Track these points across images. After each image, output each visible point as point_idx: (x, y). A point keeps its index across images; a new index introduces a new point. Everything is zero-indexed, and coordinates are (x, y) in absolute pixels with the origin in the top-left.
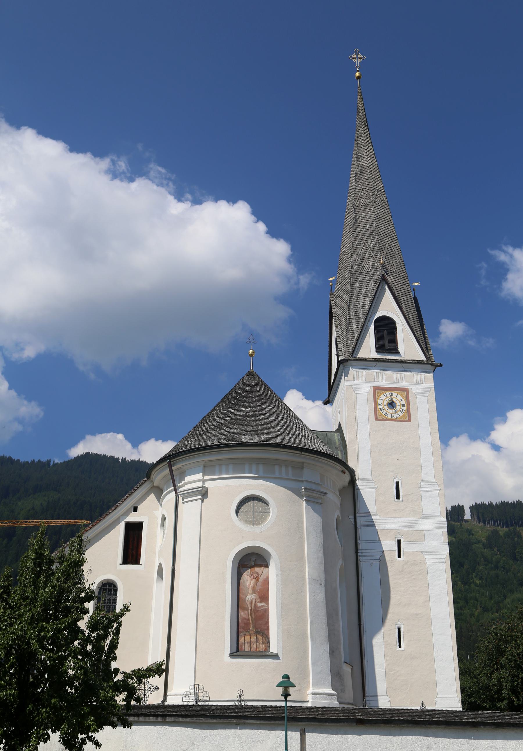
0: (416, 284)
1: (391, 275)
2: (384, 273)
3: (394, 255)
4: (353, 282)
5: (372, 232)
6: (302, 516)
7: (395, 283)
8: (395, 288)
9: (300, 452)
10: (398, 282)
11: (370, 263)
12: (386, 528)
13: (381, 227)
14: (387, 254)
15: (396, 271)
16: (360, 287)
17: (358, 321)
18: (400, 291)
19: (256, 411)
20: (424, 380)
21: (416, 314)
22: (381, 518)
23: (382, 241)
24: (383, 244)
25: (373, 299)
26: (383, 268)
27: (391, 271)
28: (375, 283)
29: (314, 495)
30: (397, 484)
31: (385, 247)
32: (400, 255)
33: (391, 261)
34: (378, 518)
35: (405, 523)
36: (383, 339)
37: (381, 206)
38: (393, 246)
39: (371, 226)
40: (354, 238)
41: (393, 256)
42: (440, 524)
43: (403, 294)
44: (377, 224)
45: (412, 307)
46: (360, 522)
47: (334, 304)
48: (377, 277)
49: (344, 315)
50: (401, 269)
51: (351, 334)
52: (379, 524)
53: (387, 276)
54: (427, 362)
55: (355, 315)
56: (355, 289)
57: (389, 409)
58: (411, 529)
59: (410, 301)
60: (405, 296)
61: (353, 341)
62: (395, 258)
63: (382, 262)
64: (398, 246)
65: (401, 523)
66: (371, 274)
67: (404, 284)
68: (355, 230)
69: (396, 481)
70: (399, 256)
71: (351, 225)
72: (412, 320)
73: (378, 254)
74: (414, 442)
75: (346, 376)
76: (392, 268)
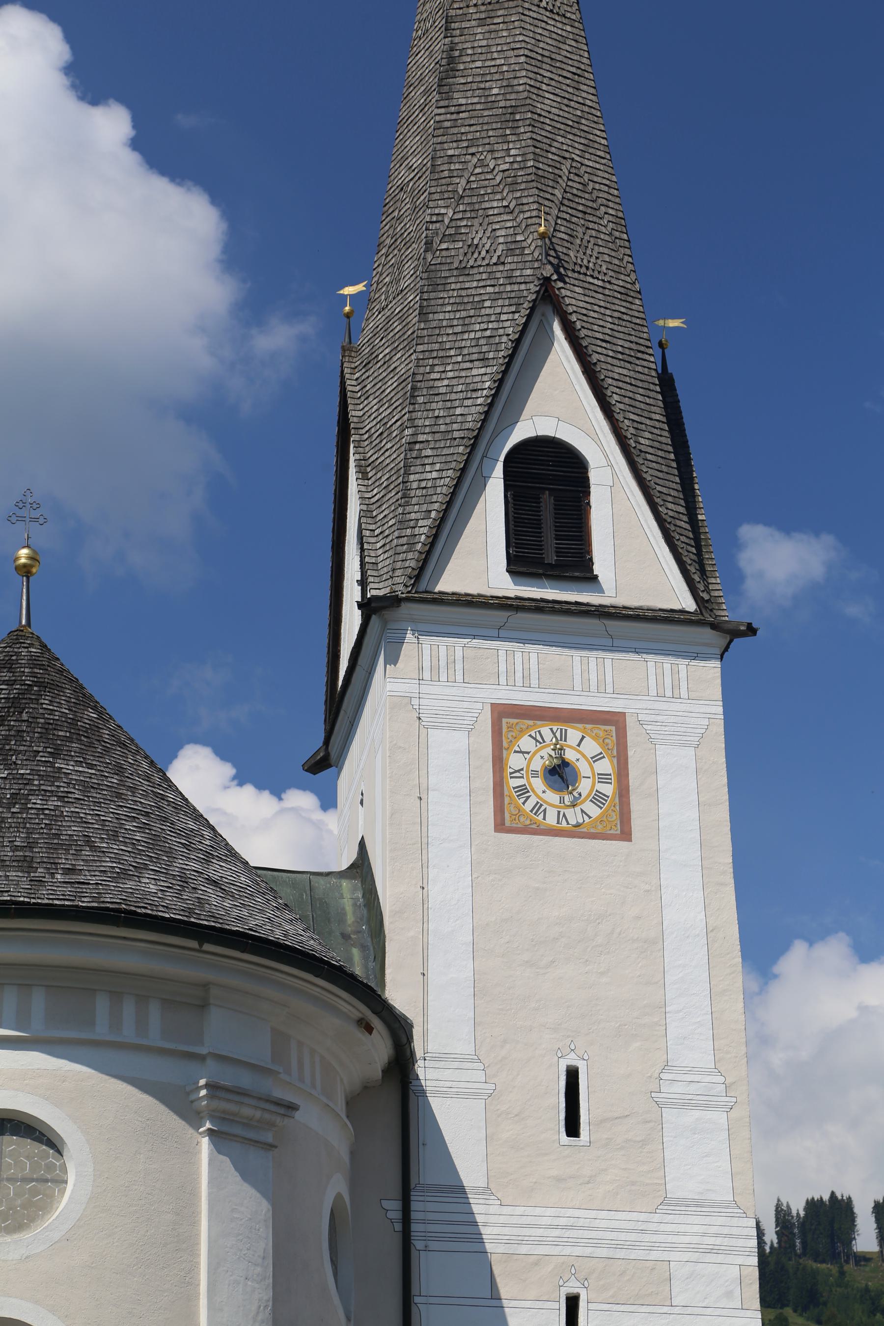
0: (673, 323)
1: (576, 283)
2: (548, 271)
3: (590, 204)
4: (432, 302)
5: (510, 110)
6: (194, 1194)
7: (592, 314)
8: (590, 333)
9: (194, 944)
10: (602, 310)
11: (498, 233)
12: (524, 1249)
13: (547, 95)
14: (566, 202)
15: (598, 267)
16: (455, 322)
17: (445, 451)
18: (608, 346)
19: (29, 782)
20: (684, 685)
21: (666, 434)
22: (506, 1210)
23: (545, 147)
24: (550, 162)
25: (505, 373)
26: (548, 255)
27: (577, 268)
28: (513, 309)
29: (247, 1111)
30: (572, 1076)
31: (556, 171)
32: (616, 207)
33: (581, 230)
34: (492, 1209)
35: (597, 1229)
36: (538, 524)
37: (551, 11)
38: (589, 170)
39: (510, 90)
40: (441, 132)
41: (589, 211)
42: (730, 1236)
43: (620, 356)
44: (532, 83)
45: (653, 409)
46: (424, 1222)
47: (358, 388)
48: (523, 287)
49: (394, 428)
50: (616, 262)
51: (414, 501)
52: (496, 1230)
53: (560, 284)
54: (701, 617)
55: (435, 429)
56: (437, 331)
57: (574, 760)
58: (620, 1254)
59: (646, 385)
60: (628, 365)
61: (423, 530)
62: (594, 219)
63: (542, 229)
64: (610, 170)
65: (582, 1228)
66: (498, 275)
67: (625, 317)
68: (445, 103)
69: (568, 1067)
70: (611, 211)
71: (433, 80)
72: (649, 457)
73: (531, 200)
74: (638, 918)
75: (393, 659)
76: (580, 255)
